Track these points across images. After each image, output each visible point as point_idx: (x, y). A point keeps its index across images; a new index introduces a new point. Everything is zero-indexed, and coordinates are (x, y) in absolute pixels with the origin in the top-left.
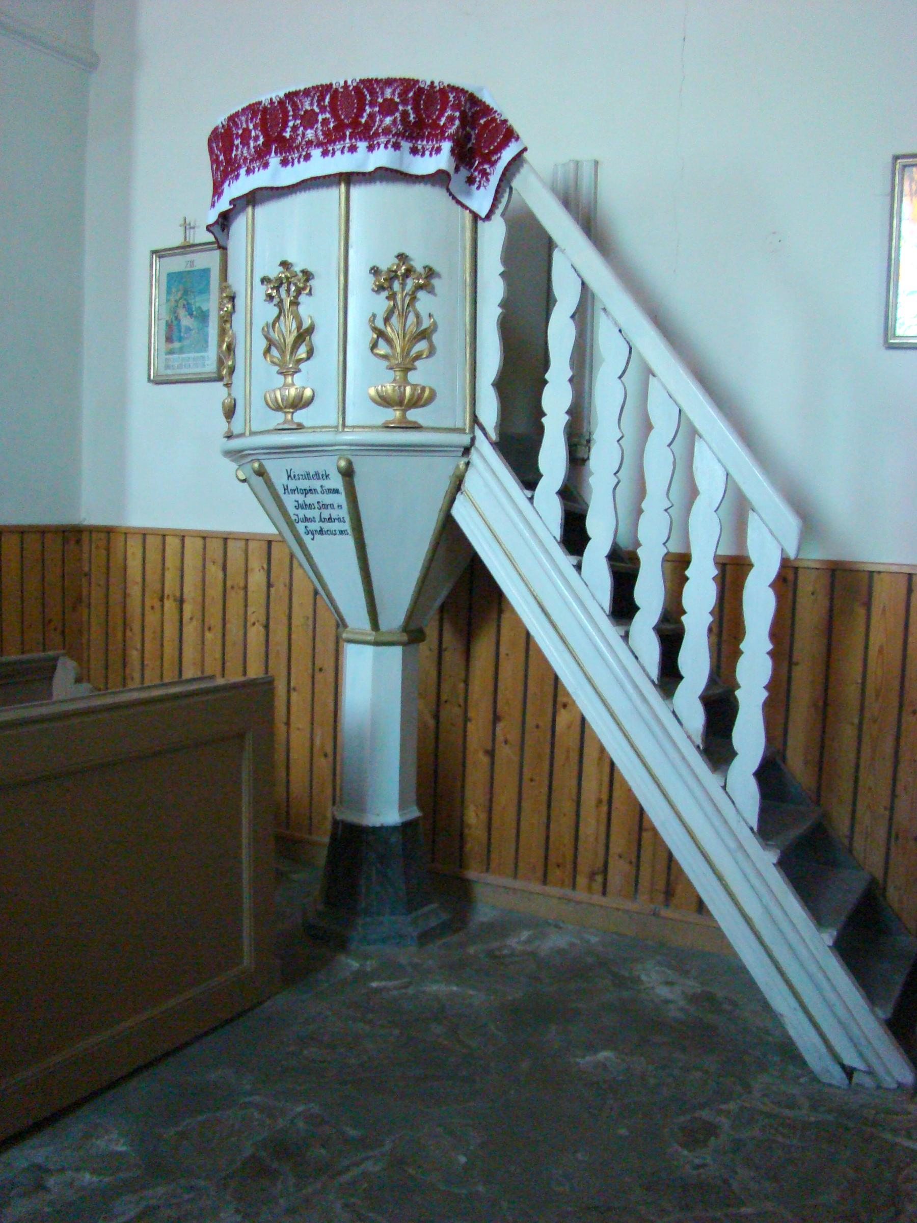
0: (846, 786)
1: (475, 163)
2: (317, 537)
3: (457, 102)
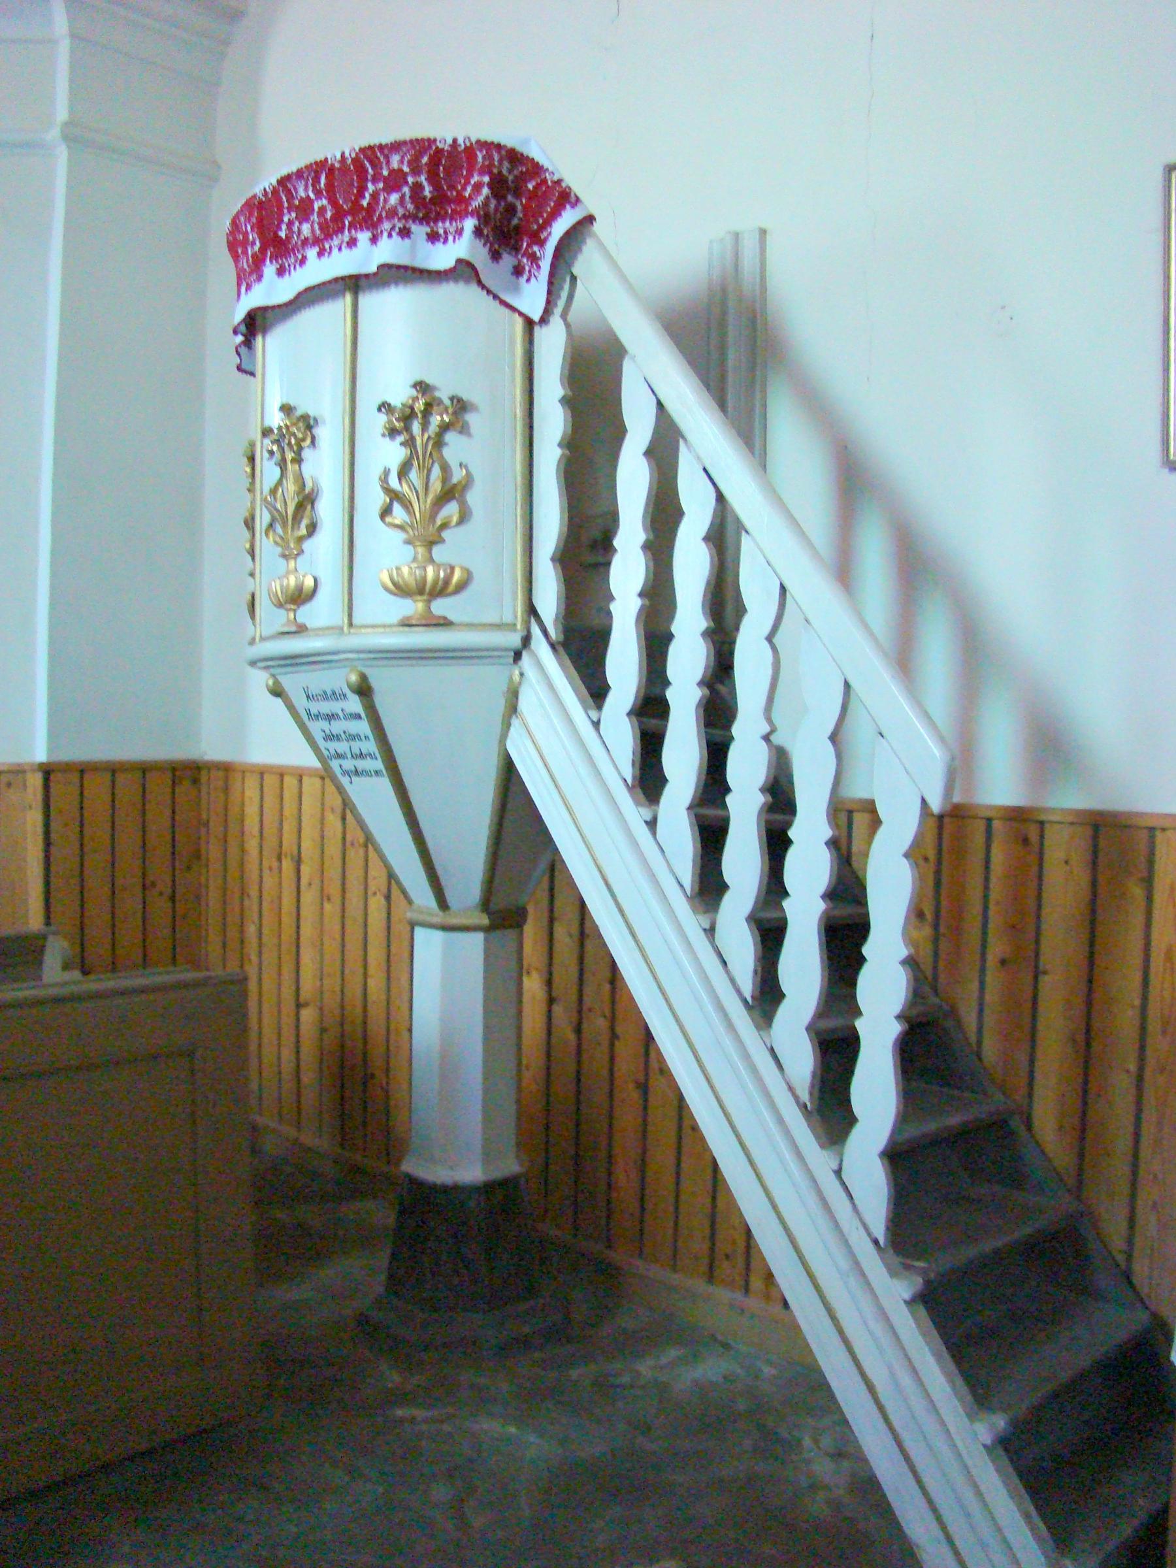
0: (1119, 1168)
1: (522, 245)
2: (355, 779)
3: (487, 163)
